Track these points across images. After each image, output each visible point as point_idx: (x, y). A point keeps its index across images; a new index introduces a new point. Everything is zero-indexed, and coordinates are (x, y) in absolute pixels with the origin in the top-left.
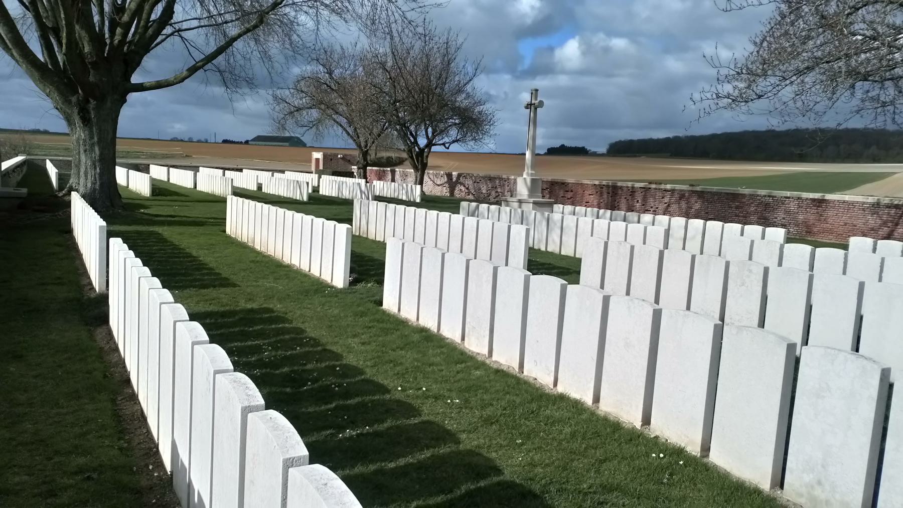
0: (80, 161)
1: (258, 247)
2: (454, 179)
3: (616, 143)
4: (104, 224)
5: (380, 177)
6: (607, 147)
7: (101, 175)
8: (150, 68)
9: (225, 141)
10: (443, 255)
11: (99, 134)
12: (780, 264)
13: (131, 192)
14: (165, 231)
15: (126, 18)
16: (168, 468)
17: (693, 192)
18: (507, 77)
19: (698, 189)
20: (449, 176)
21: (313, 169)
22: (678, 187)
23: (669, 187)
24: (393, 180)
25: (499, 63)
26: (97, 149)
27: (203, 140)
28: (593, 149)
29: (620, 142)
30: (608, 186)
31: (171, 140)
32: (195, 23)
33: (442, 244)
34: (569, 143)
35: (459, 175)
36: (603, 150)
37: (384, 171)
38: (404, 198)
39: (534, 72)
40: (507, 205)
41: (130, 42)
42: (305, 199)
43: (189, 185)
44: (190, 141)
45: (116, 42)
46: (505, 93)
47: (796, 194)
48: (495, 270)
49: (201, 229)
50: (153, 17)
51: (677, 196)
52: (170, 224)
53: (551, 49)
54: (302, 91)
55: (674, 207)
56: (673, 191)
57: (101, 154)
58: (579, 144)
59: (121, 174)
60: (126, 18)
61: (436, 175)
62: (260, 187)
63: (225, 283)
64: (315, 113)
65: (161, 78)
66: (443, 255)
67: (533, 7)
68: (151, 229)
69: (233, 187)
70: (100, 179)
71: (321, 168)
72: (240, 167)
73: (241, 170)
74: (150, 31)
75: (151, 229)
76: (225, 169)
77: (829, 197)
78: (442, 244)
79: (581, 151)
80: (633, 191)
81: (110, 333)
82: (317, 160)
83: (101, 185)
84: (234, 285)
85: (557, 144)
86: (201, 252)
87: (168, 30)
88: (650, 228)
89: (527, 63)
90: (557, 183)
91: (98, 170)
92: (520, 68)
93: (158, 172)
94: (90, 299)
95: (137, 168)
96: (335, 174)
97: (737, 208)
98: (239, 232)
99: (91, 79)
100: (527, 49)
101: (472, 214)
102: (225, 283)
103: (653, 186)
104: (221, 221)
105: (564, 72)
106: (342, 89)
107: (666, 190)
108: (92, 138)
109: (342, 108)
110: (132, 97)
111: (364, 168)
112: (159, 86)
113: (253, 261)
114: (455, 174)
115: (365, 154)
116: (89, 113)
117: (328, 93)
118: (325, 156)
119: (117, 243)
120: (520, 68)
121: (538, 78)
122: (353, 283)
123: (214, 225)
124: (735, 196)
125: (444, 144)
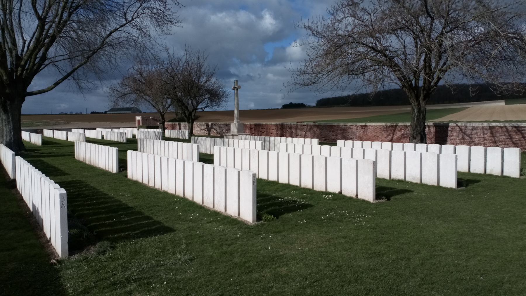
2: (210, 126)
3: (321, 100)
4: (14, 153)
6: (316, 102)
7: (14, 135)
10: (239, 172)
12: (330, 156)
13: (32, 144)
14: (45, 160)
15: (23, 63)
17: (316, 125)
18: (259, 65)
19: (317, 124)
20: (207, 125)
21: (137, 125)
22: (309, 123)
23: (305, 124)
24: (180, 129)
27: (79, 113)
28: (308, 104)
29: (323, 99)
30: (280, 125)
31: (60, 114)
32: (62, 58)
34: (295, 102)
35: (212, 124)
36: (314, 104)
37: (175, 124)
38: (181, 138)
39: (275, 61)
40: (227, 138)
41: (27, 69)
43: (64, 138)
45: (18, 74)
46: (259, 74)
47: (355, 123)
48: (184, 162)
49: (63, 158)
51: (309, 128)
53: (284, 48)
54: (126, 85)
55: (308, 133)
56: (307, 125)
57: (13, 126)
58: (300, 102)
60: (23, 63)
61: (201, 125)
62: (103, 137)
63: (65, 174)
65: (41, 88)
67: (271, 24)
69: (86, 138)
70: (14, 137)
71: (141, 124)
72: (94, 127)
73: (95, 129)
74: (35, 67)
77: (368, 124)
78: (238, 166)
80: (290, 127)
82: (139, 121)
84: (69, 175)
85: (287, 102)
87: (47, 62)
89: (270, 56)
90: (257, 125)
91: (12, 133)
92: (266, 60)
93: (48, 133)
95: (36, 132)
98: (97, 162)
99: (7, 91)
100: (270, 49)
102: (65, 174)
103: (299, 124)
104: (73, 154)
105: (291, 61)
106: (149, 83)
107: (304, 125)
108: (8, 118)
109: (149, 92)
110: (27, 98)
111: (163, 123)
113: (82, 167)
114: (210, 123)
115: (163, 116)
117: (141, 85)
119: (18, 159)
120: (266, 60)
122: (120, 171)
123: (69, 155)
124: (331, 127)
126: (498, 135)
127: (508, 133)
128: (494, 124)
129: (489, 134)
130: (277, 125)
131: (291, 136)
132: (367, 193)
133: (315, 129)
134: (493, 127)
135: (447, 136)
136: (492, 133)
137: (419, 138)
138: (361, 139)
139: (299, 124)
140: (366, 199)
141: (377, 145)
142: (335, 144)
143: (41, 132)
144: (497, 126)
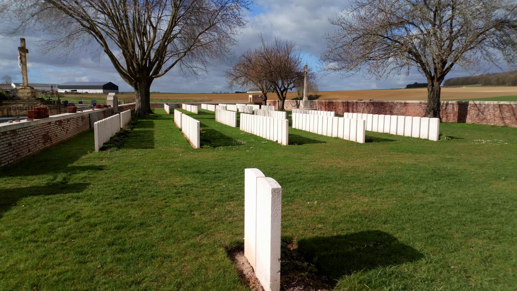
17: (371, 103)
31: (212, 93)
72: (371, 145)
73: (235, 104)
80: (353, 104)
85: (412, 82)
93: (204, 107)
97: (384, 108)
127: (513, 111)
129: (498, 111)
130: (343, 102)
131: (353, 112)
132: (361, 140)
133: (371, 106)
134: (502, 105)
136: (500, 111)
137: (432, 113)
138: (403, 114)
139: (359, 101)
140: (273, 138)
141: (365, 115)
142: (342, 116)
143: (199, 105)
144: (504, 105)
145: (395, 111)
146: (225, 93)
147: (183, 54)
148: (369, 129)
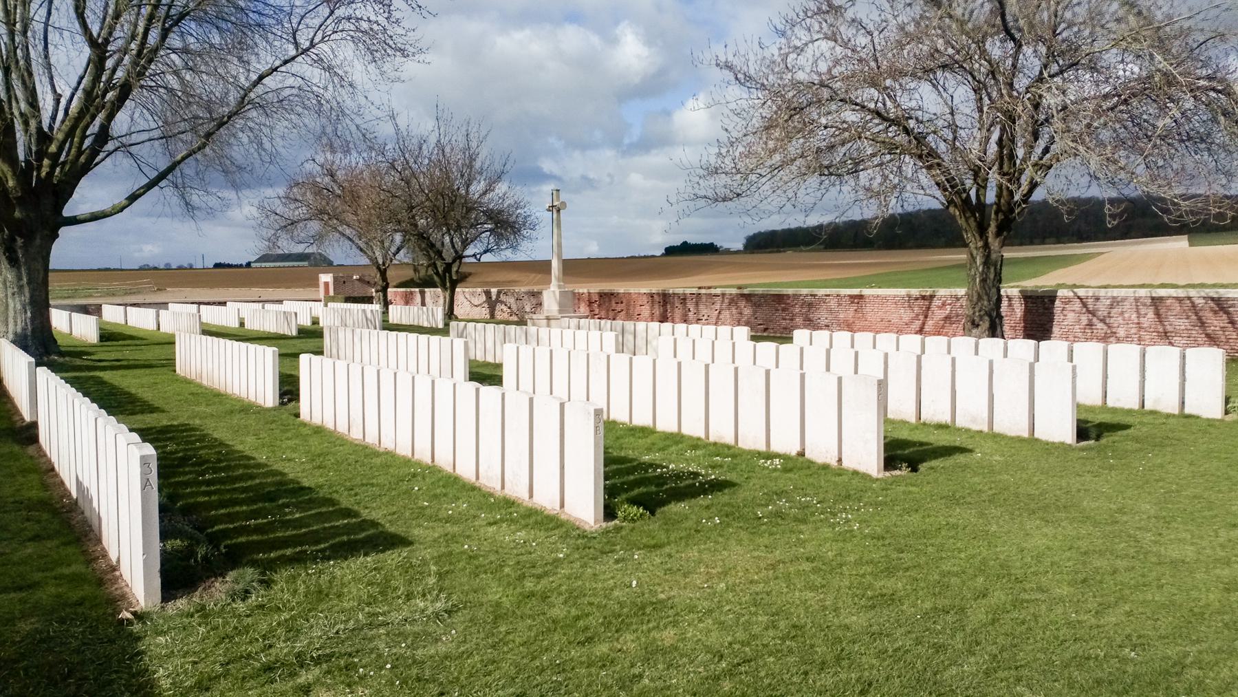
0: (7, 306)
1: (205, 383)
2: (494, 297)
5: (408, 300)
6: (744, 241)
7: (33, 319)
8: (88, 195)
9: (217, 266)
10: (562, 405)
11: (29, 274)
14: (107, 376)
15: (53, 148)
16: (74, 494)
17: (743, 295)
18: (609, 153)
19: (746, 291)
20: (488, 294)
22: (728, 291)
23: (718, 291)
24: (423, 304)
25: (598, 135)
26: (26, 290)
28: (726, 245)
29: (760, 234)
31: (141, 269)
32: (145, 136)
33: (526, 384)
34: (694, 239)
35: (499, 293)
36: (739, 245)
37: (411, 293)
38: (426, 324)
40: (534, 325)
42: (294, 333)
43: (151, 326)
44: (155, 268)
46: (609, 175)
48: (433, 382)
49: (148, 371)
50: (84, 147)
51: (726, 301)
52: (113, 368)
53: (667, 113)
56: (723, 295)
57: (31, 297)
58: (705, 240)
59: (59, 320)
60: (53, 148)
61: (473, 294)
63: (152, 409)
64: (315, 226)
66: (562, 405)
68: (92, 374)
69: (201, 323)
70: (32, 323)
71: (332, 293)
72: (222, 300)
74: (82, 159)
75: (92, 374)
76: (200, 303)
77: (866, 292)
78: (560, 390)
79: (710, 249)
80: (684, 299)
81: (40, 448)
82: (326, 284)
83: (33, 331)
85: (677, 241)
86: (140, 391)
87: (110, 146)
88: (807, 349)
89: (635, 134)
90: (605, 294)
91: (29, 314)
93: (113, 314)
94: (22, 427)
96: (350, 299)
97: (784, 310)
101: (460, 335)
102: (152, 409)
103: (703, 291)
104: (170, 363)
106: (351, 196)
108: (20, 278)
110: (64, 231)
111: (384, 290)
112: (94, 217)
114: (494, 291)
116: (15, 252)
117: (333, 201)
118: (335, 279)
120: (626, 141)
121: (654, 151)
125: (474, 255)
126: (1172, 319)
127: (1196, 314)
128: (1162, 292)
130: (652, 295)
132: (865, 456)
133: (742, 304)
134: (1161, 299)
135: (1052, 321)
136: (1158, 314)
137: (985, 324)
138: (850, 327)
139: (703, 291)
143: (96, 310)
145: (822, 316)
146: (180, 268)
147: (316, 40)
148: (902, 407)
